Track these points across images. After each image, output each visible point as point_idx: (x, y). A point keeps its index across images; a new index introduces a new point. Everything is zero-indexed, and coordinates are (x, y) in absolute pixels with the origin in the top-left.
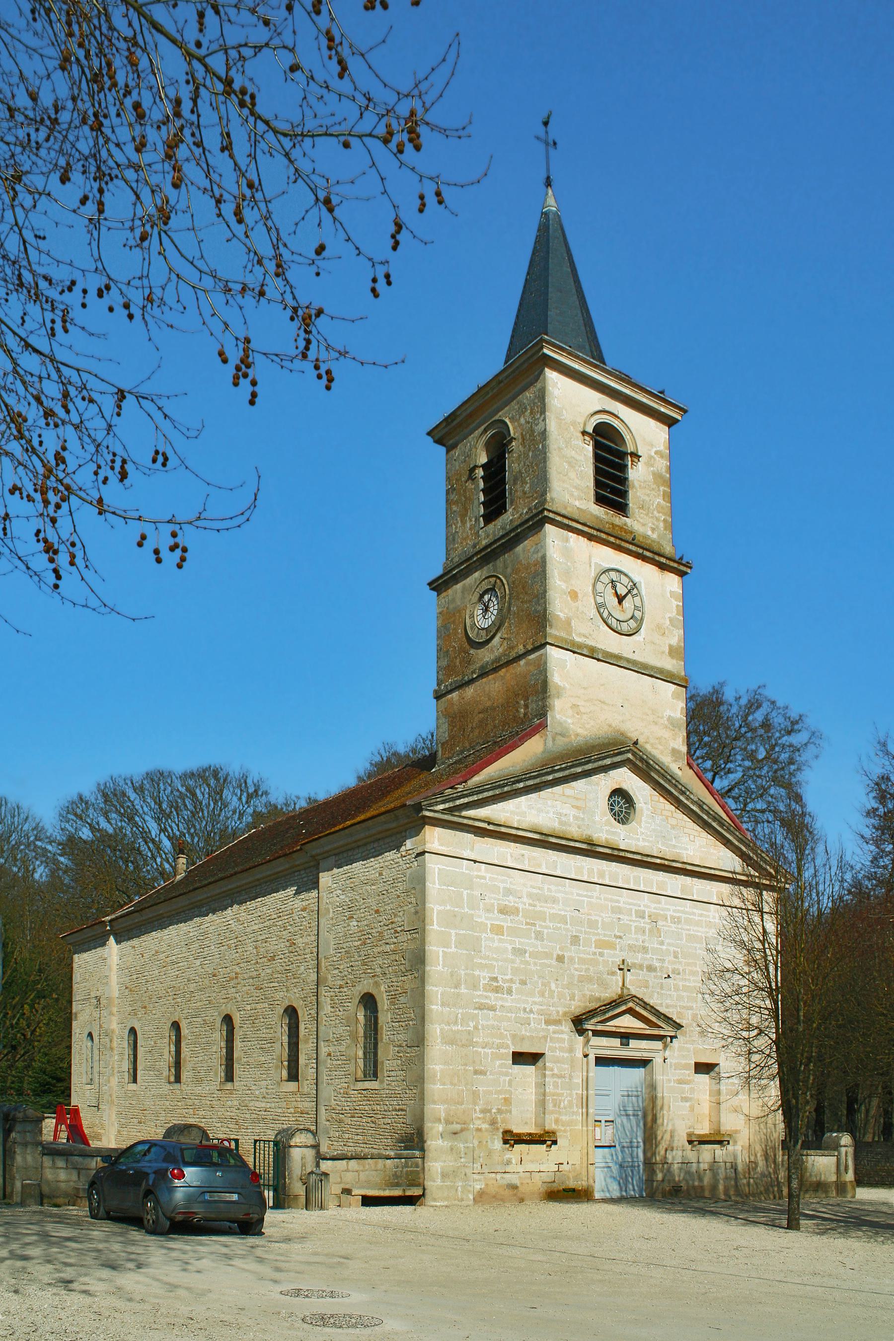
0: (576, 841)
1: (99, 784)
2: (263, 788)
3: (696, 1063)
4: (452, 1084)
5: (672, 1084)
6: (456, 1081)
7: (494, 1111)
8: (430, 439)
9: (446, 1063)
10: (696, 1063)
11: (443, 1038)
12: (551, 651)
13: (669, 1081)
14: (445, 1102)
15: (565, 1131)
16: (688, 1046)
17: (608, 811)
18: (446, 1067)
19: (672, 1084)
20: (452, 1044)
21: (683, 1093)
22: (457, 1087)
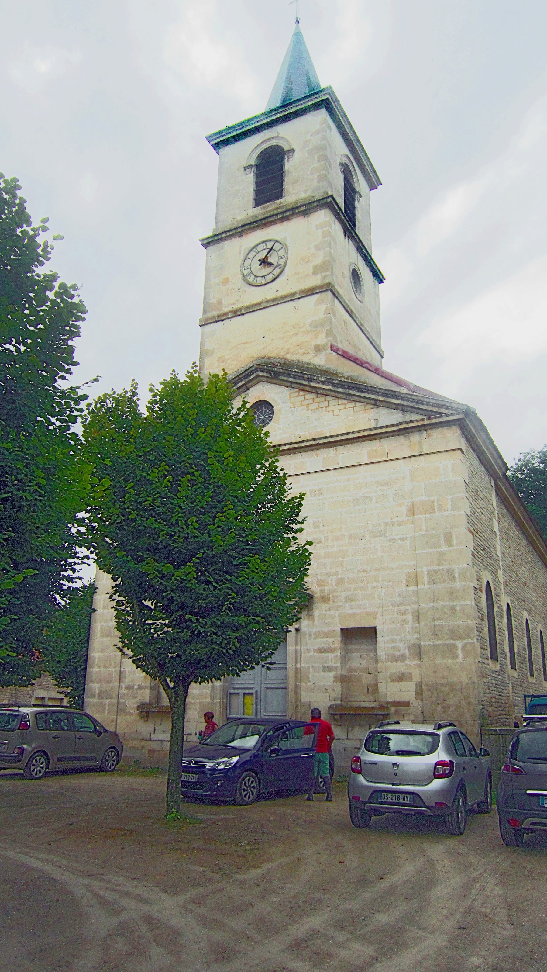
0: (230, 703)
1: (361, 196)
2: (259, 263)
3: (342, 629)
4: (105, 667)
5: (312, 654)
6: (107, 665)
7: (136, 687)
8: (200, 243)
9: (102, 651)
10: (342, 629)
11: (102, 633)
12: (361, 775)
13: (308, 650)
14: (100, 681)
15: (194, 703)
16: (332, 612)
17: (272, 421)
18: (103, 654)
19: (312, 654)
20: (107, 636)
21: (325, 662)
22: (108, 669)
